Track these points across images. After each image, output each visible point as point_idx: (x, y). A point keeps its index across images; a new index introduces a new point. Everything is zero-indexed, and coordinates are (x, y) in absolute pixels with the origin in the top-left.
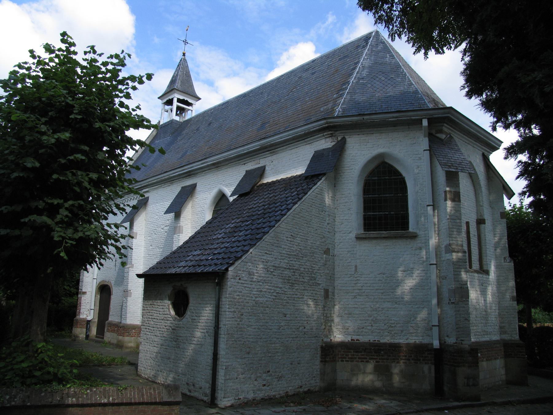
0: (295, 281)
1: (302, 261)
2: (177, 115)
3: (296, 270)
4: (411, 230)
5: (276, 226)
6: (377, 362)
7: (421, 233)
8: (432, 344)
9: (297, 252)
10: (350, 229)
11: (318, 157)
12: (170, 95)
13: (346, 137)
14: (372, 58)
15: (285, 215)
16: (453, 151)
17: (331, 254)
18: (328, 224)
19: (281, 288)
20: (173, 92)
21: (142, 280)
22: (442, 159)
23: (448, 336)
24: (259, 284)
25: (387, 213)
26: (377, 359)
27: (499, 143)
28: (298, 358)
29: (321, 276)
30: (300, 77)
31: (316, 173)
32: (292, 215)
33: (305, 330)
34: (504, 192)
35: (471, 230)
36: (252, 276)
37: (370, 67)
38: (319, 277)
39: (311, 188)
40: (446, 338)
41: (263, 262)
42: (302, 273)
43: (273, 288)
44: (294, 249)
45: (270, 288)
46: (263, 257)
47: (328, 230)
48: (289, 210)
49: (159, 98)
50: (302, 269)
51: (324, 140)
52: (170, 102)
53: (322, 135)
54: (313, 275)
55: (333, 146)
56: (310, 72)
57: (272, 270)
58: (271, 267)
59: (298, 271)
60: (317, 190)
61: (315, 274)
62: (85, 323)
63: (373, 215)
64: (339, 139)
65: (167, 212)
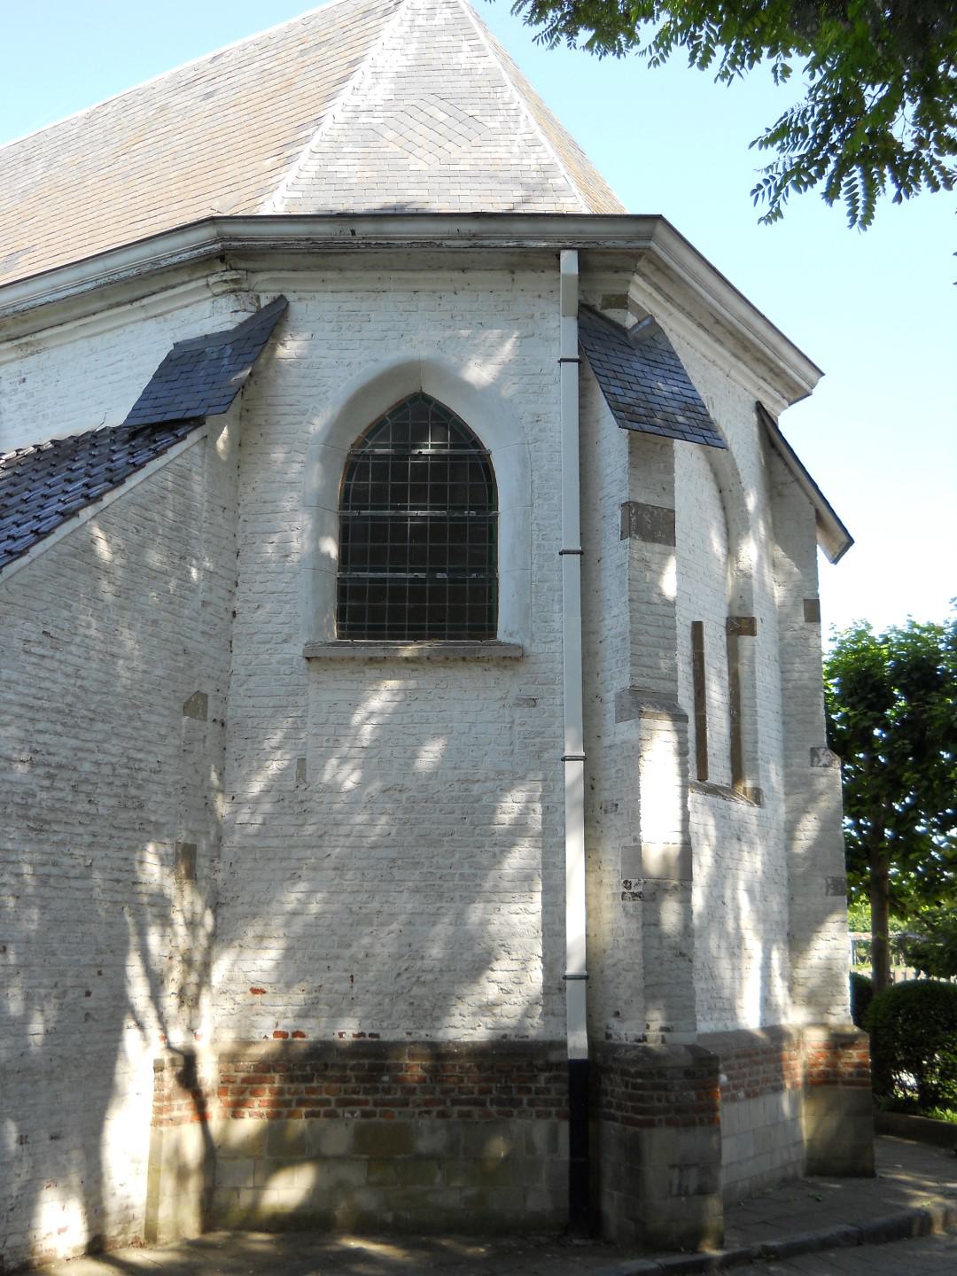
1: (89, 736)
3: (60, 766)
4: (501, 636)
6: (365, 1115)
7: (534, 648)
8: (563, 1045)
9: (69, 699)
10: (286, 630)
11: (183, 363)
13: (290, 297)
14: (412, 49)
15: (22, 553)
16: (657, 371)
17: (210, 715)
18: (205, 604)
22: (619, 391)
23: (617, 1014)
25: (422, 575)
26: (366, 1103)
27: (811, 374)
28: (52, 1114)
29: (168, 795)
30: (162, 109)
31: (169, 417)
32: (53, 555)
33: (89, 1003)
34: (819, 536)
35: (707, 650)
37: (399, 76)
38: (159, 798)
39: (142, 466)
40: (613, 1022)
42: (87, 781)
44: (57, 689)
47: (201, 627)
48: (40, 535)
50: (87, 767)
51: (207, 305)
53: (202, 282)
54: (133, 791)
55: (242, 325)
56: (200, 89)
59: (66, 774)
61: (139, 787)
63: (372, 580)
64: (264, 302)
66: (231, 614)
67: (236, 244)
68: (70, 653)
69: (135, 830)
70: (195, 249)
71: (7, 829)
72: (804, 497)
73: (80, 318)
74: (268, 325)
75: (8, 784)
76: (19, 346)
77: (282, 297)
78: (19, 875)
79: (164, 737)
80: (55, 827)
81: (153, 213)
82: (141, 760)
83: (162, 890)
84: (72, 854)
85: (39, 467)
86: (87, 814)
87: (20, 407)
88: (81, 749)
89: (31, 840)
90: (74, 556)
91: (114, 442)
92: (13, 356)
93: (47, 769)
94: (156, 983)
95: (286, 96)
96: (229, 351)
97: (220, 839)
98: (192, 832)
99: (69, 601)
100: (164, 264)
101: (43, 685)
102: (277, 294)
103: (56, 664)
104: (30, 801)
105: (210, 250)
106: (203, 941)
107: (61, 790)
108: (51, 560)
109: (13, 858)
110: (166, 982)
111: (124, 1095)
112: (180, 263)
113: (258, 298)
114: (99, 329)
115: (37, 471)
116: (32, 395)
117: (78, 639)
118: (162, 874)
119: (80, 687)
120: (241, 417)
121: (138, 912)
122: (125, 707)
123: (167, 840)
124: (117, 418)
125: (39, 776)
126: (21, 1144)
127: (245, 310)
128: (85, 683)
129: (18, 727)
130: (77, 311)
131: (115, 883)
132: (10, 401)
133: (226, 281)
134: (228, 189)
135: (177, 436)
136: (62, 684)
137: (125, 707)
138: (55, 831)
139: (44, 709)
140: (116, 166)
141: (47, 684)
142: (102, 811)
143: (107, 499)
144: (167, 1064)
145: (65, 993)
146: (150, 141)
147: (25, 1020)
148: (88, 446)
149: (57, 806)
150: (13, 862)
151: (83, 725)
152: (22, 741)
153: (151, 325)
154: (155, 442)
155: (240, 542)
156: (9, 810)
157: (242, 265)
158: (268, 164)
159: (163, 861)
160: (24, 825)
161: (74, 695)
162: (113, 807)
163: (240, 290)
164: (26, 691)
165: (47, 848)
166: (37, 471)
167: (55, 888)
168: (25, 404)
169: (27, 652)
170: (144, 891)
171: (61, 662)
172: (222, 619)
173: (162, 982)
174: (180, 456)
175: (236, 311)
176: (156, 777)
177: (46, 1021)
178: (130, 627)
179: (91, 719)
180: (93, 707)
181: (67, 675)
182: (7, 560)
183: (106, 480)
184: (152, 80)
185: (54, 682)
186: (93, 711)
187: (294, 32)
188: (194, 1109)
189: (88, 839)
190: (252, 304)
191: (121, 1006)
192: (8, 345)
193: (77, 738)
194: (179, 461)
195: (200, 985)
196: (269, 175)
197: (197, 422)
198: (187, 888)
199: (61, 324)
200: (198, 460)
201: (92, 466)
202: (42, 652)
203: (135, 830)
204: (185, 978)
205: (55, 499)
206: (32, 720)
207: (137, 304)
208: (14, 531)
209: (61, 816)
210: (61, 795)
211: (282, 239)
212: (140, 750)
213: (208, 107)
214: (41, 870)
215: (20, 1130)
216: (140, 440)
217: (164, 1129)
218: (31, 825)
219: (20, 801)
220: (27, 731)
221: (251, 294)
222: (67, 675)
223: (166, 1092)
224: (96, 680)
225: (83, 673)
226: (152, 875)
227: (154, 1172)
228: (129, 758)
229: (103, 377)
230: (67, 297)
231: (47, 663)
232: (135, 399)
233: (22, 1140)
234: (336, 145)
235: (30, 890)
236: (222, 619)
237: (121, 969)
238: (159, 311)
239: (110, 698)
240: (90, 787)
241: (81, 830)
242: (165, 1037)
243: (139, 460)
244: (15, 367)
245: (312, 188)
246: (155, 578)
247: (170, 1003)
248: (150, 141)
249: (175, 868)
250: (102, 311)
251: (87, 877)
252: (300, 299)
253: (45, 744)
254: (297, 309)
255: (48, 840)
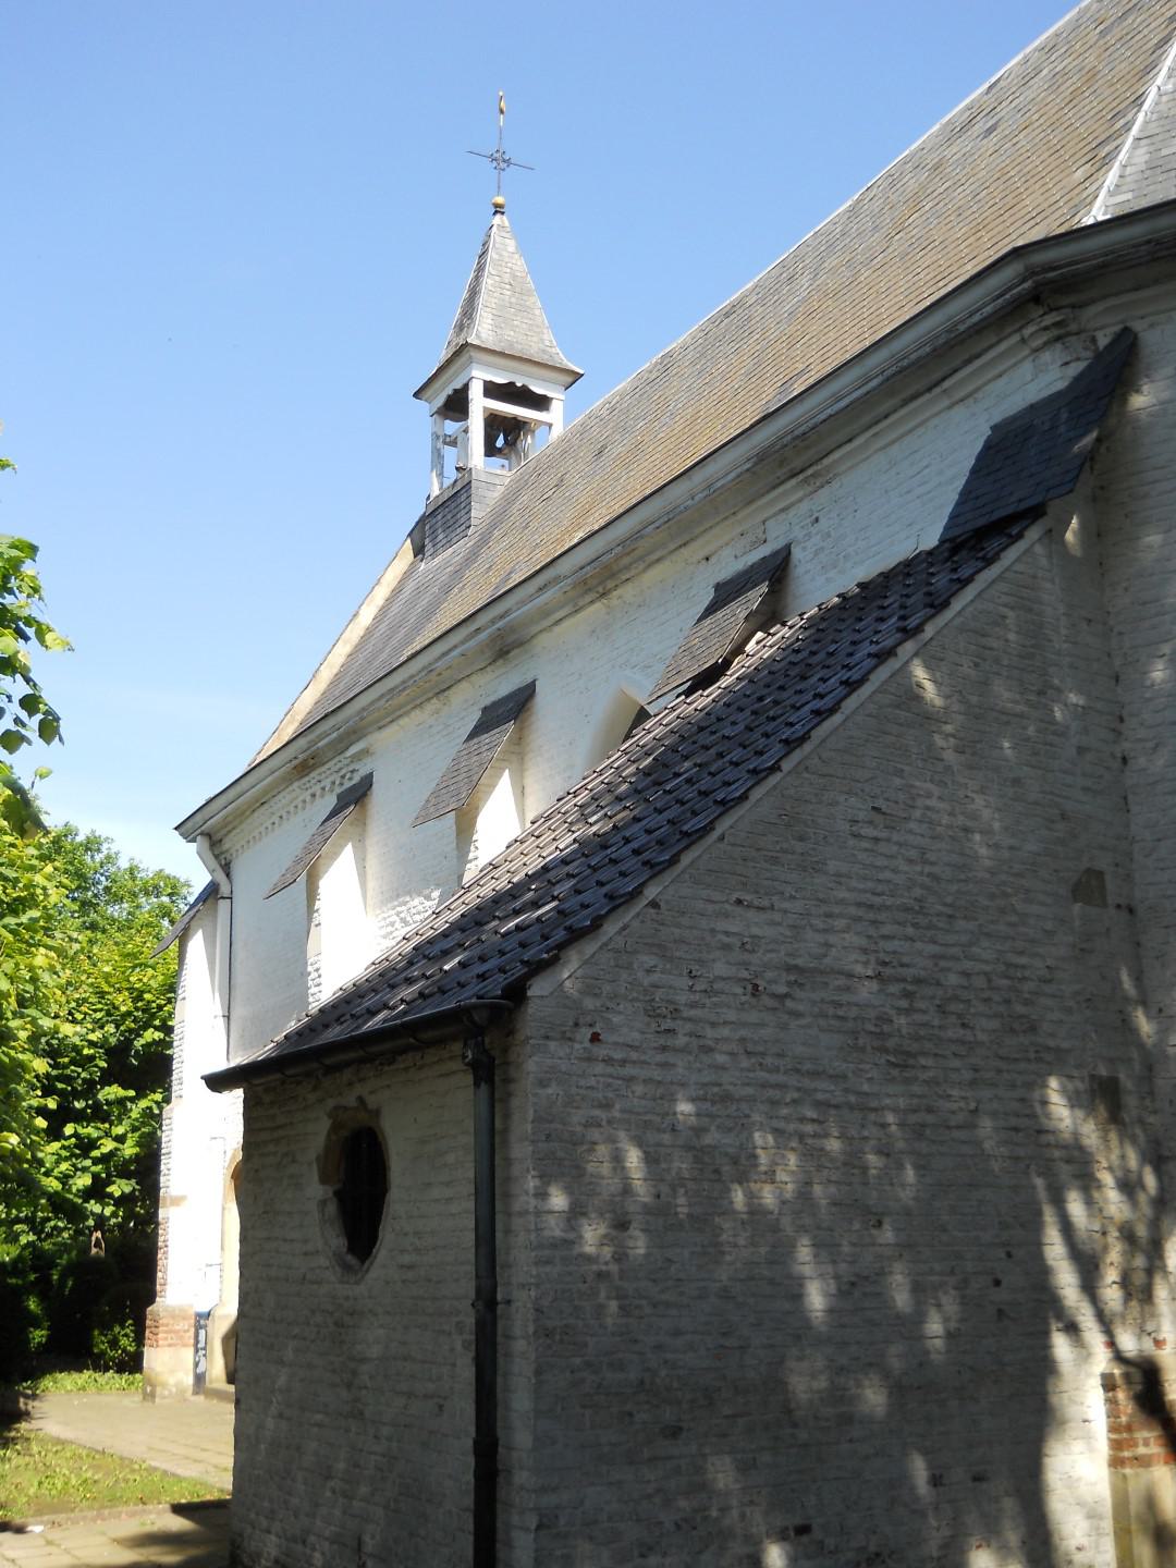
0: (917, 1038)
2: (491, 450)
3: (918, 981)
5: (786, 765)
9: (918, 892)
11: (1005, 449)
12: (457, 374)
13: (1137, 326)
15: (833, 710)
17: (1110, 900)
18: (1081, 750)
19: (834, 1078)
20: (463, 359)
21: (235, 1098)
24: (706, 1059)
29: (1069, 1011)
36: (668, 1024)
41: (726, 947)
42: (956, 998)
43: (793, 1080)
45: (774, 1078)
46: (721, 925)
48: (852, 686)
49: (417, 395)
50: (953, 979)
51: (1027, 366)
52: (456, 406)
53: (1016, 338)
54: (1020, 1009)
55: (1078, 379)
56: (979, 128)
57: (782, 989)
58: (770, 975)
60: (1002, 587)
61: (1026, 1003)
62: (187, 1326)
64: (1103, 341)
65: (422, 819)
66: (1120, 760)
67: (1051, 275)
68: (910, 832)
69: (1029, 1060)
70: (998, 297)
71: (861, 1066)
72: (519, 1399)
73: (870, 427)
74: (1116, 369)
75: (855, 1008)
76: (805, 481)
77: (1126, 330)
78: (884, 1126)
79: (1049, 933)
80: (923, 1061)
81: (941, 284)
82: (1024, 967)
83: (1076, 1139)
84: (950, 1096)
85: (845, 616)
86: (963, 1043)
87: (816, 553)
88: (943, 957)
89: (894, 1078)
90: (898, 707)
91: (931, 565)
92: (800, 494)
93: (902, 985)
94: (1088, 1268)
95: (1089, 91)
96: (1064, 416)
97: (1150, 1068)
98: (1111, 1061)
99: (899, 766)
100: (962, 328)
101: (881, 876)
102: (1117, 328)
103: (895, 848)
104: (886, 1028)
105: (1019, 292)
106: (1146, 1209)
107: (924, 1012)
108: (869, 715)
109: (874, 1104)
110: (1102, 1266)
111: (1063, 1422)
112: (982, 320)
113: (1094, 340)
114: (894, 436)
115: (843, 620)
116: (829, 535)
117: (917, 814)
118: (1074, 1118)
119: (929, 875)
120: (1094, 499)
121: (1048, 1172)
122: (992, 897)
123: (1075, 1073)
124: (931, 540)
125: (893, 995)
126: (935, 1485)
127: (1078, 359)
128: (935, 869)
129: (858, 933)
130: (866, 419)
131: (1013, 1133)
132: (804, 549)
133: (1046, 328)
134: (1032, 222)
135: (1010, 536)
136: (906, 873)
137: (992, 897)
138: (924, 1067)
139: (888, 908)
140: (890, 250)
141: (887, 875)
142: (981, 1037)
143: (929, 630)
144: (1119, 1381)
145: (966, 1281)
146: (927, 208)
147: (919, 1318)
148: (901, 578)
149: (922, 1033)
150: (875, 1110)
151: (941, 925)
152: (865, 951)
153: (959, 412)
154: (983, 549)
155: (1117, 662)
156: (861, 1042)
157: (1066, 300)
158: (1080, 175)
159: (1074, 1101)
160: (883, 1061)
161: (923, 886)
162: (994, 1031)
163: (1069, 334)
164: (861, 886)
165: (916, 1089)
166: (843, 620)
167: (934, 1142)
168: (822, 548)
169: (856, 836)
170: (1053, 1142)
171: (900, 844)
172: (1108, 768)
173: (1097, 1267)
174: (1017, 560)
175: (1067, 364)
176: (1047, 988)
177: (946, 1320)
178: (982, 791)
179: (950, 916)
180: (949, 900)
181: (911, 861)
182: (815, 721)
183: (926, 606)
184: (920, 141)
185: (895, 871)
186: (950, 905)
187: (1088, 15)
188: (1166, 1445)
189: (967, 1075)
190: (1086, 349)
191: (1045, 1309)
192: (793, 482)
193: (935, 943)
194: (1019, 567)
195: (1150, 1272)
196: (1083, 186)
197: (1035, 513)
198: (1113, 1136)
199: (850, 440)
200: (1044, 562)
201: (907, 596)
202: (875, 833)
203: (1029, 1060)
204: (1129, 1261)
205: (867, 643)
206: (874, 922)
207: (937, 390)
208: (822, 689)
209: (928, 1046)
210: (925, 1018)
211: (1112, 252)
212: (1021, 953)
213: (991, 144)
214: (913, 1119)
215: (931, 1466)
216: (964, 553)
217: (1128, 1471)
218: (893, 1059)
219: (873, 1029)
220: (869, 937)
221: (1083, 336)
222: (911, 861)
223: (1124, 1419)
224: (948, 865)
225: (931, 857)
226: (1061, 1120)
227: (1122, 1535)
228: (1009, 965)
229: (909, 492)
230: (851, 403)
231: (883, 848)
232: (949, 509)
233: (936, 1481)
234: (1168, 121)
235: (901, 1145)
236: (1108, 768)
237: (1037, 1247)
238: (962, 394)
239: (971, 886)
240: (961, 1006)
241: (956, 1063)
242: (1112, 1344)
243: (965, 572)
244: (804, 507)
245: (1146, 183)
246: (1008, 723)
247: (1112, 1295)
248: (927, 208)
249: (1090, 1110)
250: (895, 411)
251: (975, 1126)
252: (1152, 326)
253: (894, 952)
254: (1149, 339)
255: (916, 1079)
